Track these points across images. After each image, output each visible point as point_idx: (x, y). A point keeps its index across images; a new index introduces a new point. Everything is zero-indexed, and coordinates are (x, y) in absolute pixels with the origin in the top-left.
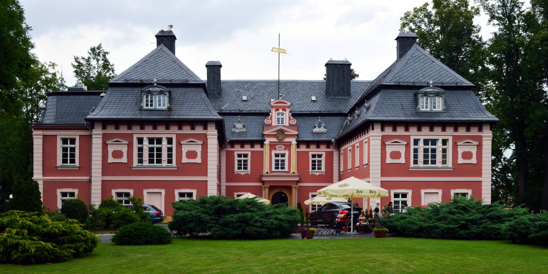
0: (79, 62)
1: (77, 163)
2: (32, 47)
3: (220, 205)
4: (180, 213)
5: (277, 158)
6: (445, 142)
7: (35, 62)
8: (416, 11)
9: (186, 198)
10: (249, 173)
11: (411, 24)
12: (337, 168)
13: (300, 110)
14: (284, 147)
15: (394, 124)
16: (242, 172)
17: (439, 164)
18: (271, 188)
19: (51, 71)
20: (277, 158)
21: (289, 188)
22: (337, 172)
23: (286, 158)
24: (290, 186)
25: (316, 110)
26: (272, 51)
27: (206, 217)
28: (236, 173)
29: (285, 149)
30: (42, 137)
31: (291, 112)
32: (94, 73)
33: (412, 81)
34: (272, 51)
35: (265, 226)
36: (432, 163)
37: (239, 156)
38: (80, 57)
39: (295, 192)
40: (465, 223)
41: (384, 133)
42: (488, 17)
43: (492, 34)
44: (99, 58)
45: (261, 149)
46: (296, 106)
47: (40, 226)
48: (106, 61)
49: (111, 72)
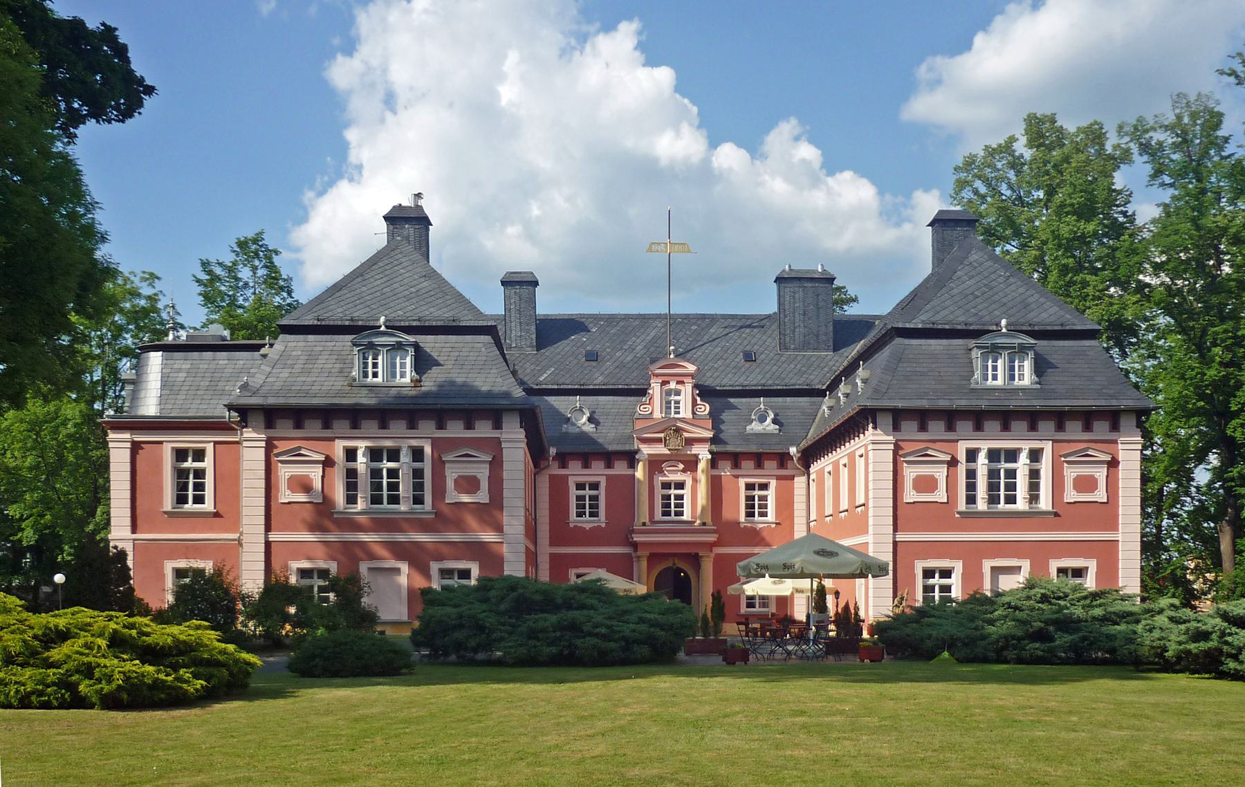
0: (210, 273)
1: (208, 506)
2: (104, 239)
3: (521, 591)
4: (438, 611)
5: (581, 492)
6: (1035, 455)
7: (110, 272)
8: (991, 152)
9: (454, 582)
10: (603, 525)
11: (979, 184)
12: (804, 513)
13: (718, 381)
14: (681, 466)
15: (923, 417)
16: (587, 522)
17: (1021, 505)
18: (654, 558)
19: (146, 291)
20: (581, 492)
21: (695, 560)
22: (804, 520)
23: (686, 492)
24: (697, 554)
25: (754, 382)
26: (650, 250)
27: (491, 620)
28: (571, 525)
29: (684, 471)
30: (129, 445)
31: (696, 386)
32: (246, 299)
33: (962, 319)
34: (650, 250)
35: (617, 636)
36: (1007, 502)
37: (580, 486)
38: (213, 260)
39: (708, 567)
40: (1042, 625)
41: (900, 436)
42: (1148, 169)
43: (1158, 205)
44: (257, 262)
45: (630, 472)
46: (708, 374)
47: (134, 632)
48: (271, 267)
49: (285, 294)
